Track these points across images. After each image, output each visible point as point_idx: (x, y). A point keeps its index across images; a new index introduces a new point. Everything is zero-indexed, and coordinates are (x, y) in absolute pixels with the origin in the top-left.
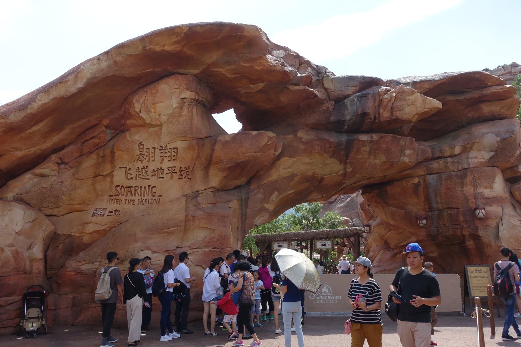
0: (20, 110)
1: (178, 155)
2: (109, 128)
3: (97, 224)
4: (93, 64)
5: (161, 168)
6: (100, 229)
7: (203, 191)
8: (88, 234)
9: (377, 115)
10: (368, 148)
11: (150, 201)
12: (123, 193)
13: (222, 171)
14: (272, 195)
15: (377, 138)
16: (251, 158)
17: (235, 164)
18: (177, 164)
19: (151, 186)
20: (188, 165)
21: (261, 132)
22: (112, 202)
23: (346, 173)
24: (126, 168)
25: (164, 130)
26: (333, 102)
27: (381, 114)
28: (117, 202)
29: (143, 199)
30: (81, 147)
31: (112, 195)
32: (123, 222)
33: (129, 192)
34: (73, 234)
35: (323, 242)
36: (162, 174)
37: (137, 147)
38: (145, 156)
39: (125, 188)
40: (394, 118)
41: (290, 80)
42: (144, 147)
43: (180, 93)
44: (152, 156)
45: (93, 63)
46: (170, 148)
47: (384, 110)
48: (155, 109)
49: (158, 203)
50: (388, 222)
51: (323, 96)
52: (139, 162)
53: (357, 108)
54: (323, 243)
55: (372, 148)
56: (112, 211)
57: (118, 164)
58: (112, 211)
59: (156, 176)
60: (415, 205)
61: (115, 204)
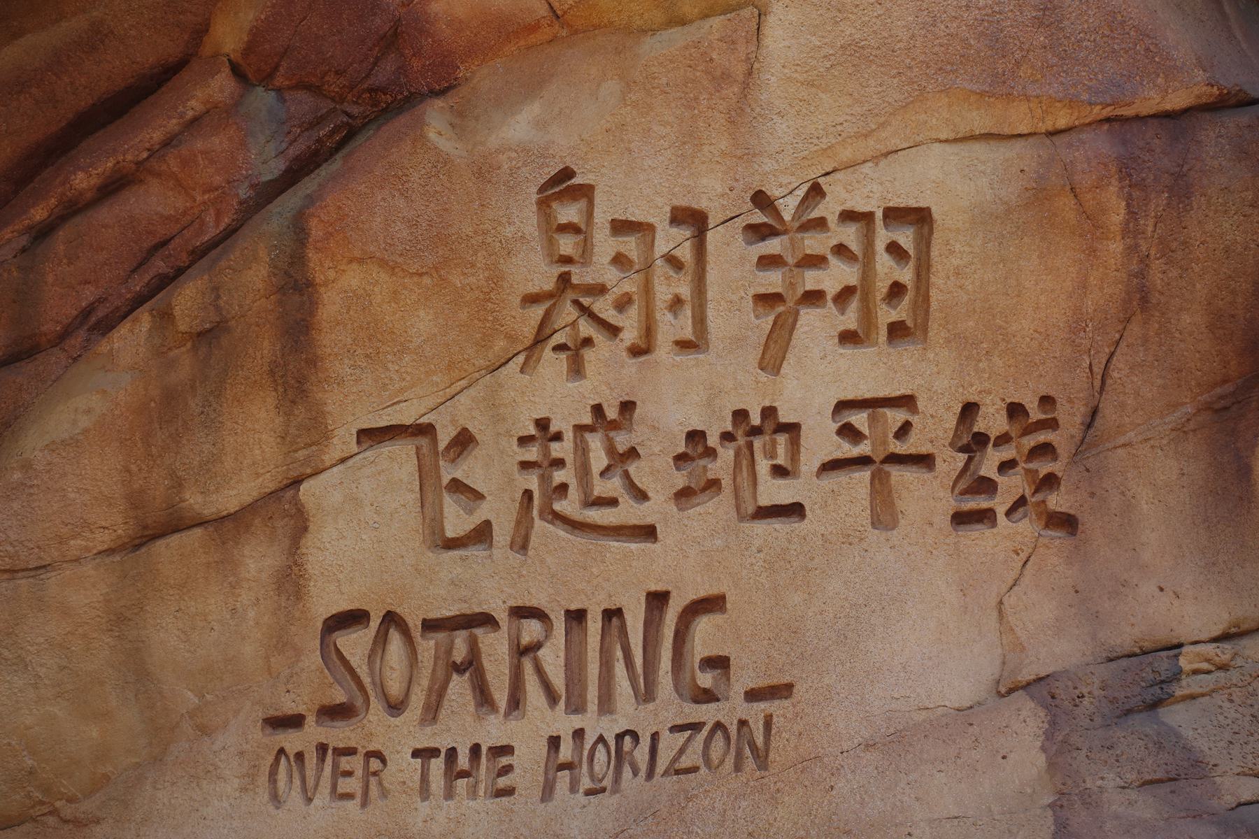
1: (937, 279)
2: (266, 79)
5: (769, 412)
7: (1210, 649)
11: (669, 744)
12: (395, 688)
19: (674, 594)
22: (297, 782)
24: (425, 430)
29: (601, 739)
31: (289, 706)
33: (459, 669)
37: (526, 219)
39: (416, 632)
42: (590, 214)
46: (848, 216)
49: (750, 763)
52: (552, 364)
59: (725, 498)
61: (322, 797)
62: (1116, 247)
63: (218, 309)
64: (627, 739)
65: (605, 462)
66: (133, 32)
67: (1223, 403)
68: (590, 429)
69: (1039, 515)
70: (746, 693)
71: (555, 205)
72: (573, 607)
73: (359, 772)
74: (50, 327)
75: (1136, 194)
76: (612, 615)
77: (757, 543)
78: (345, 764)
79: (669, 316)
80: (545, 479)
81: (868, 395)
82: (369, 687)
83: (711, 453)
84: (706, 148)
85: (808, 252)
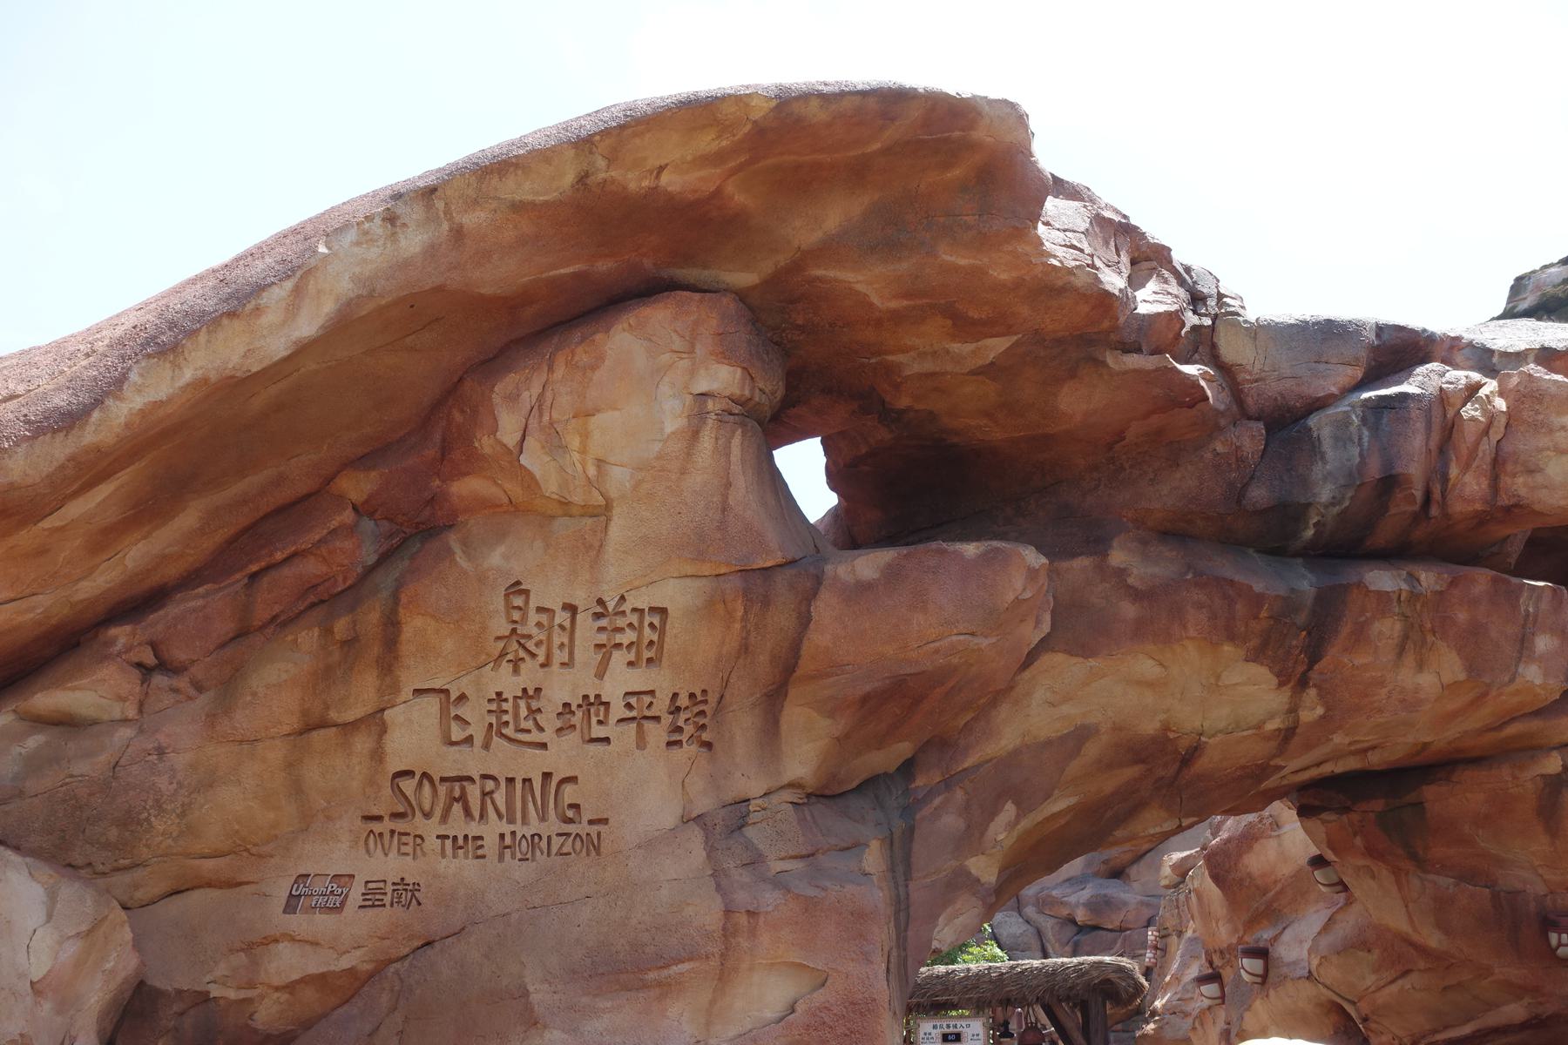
0: (55, 432)
2: (371, 515)
3: (315, 944)
4: (369, 237)
6: (332, 968)
7: (759, 801)
8: (277, 989)
9: (1439, 486)
10: (1398, 626)
13: (831, 714)
14: (992, 820)
15: (1436, 583)
16: (955, 660)
17: (887, 682)
18: (662, 681)
20: (703, 687)
21: (997, 549)
22: (379, 846)
23: (1296, 728)
24: (446, 692)
25: (618, 530)
26: (1261, 425)
27: (1453, 485)
28: (402, 847)
29: (524, 836)
30: (246, 595)
31: (375, 811)
32: (442, 939)
33: (457, 800)
34: (215, 991)
35: (948, 1026)
36: (600, 722)
37: (499, 602)
38: (533, 641)
39: (437, 783)
40: (1504, 500)
41: (1115, 328)
42: (527, 602)
43: (692, 372)
44: (562, 645)
45: (366, 233)
46: (634, 610)
47: (1466, 468)
48: (585, 435)
49: (593, 853)
50: (1415, 937)
51: (1220, 396)
53: (1361, 455)
54: (946, 1031)
55: (1412, 624)
56: (381, 885)
57: (412, 678)
58: (381, 885)
60: (1540, 865)
61: (393, 854)
62: (737, 626)
63: (355, 630)
64: (536, 837)
65: (526, 714)
66: (297, 478)
67: (771, 693)
68: (520, 698)
69: (698, 742)
70: (588, 821)
71: (511, 596)
72: (510, 776)
73: (412, 844)
74: (257, 623)
75: (748, 603)
76: (527, 781)
77: (591, 754)
78: (404, 839)
79: (559, 652)
80: (498, 718)
81: (637, 690)
82: (415, 807)
83: (573, 713)
84: (580, 578)
85: (618, 626)
